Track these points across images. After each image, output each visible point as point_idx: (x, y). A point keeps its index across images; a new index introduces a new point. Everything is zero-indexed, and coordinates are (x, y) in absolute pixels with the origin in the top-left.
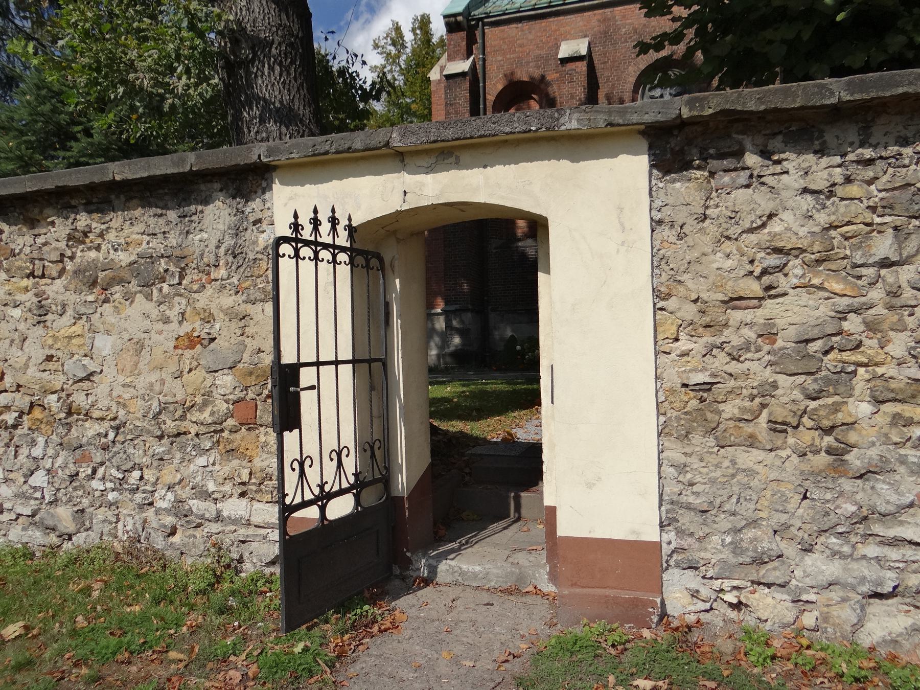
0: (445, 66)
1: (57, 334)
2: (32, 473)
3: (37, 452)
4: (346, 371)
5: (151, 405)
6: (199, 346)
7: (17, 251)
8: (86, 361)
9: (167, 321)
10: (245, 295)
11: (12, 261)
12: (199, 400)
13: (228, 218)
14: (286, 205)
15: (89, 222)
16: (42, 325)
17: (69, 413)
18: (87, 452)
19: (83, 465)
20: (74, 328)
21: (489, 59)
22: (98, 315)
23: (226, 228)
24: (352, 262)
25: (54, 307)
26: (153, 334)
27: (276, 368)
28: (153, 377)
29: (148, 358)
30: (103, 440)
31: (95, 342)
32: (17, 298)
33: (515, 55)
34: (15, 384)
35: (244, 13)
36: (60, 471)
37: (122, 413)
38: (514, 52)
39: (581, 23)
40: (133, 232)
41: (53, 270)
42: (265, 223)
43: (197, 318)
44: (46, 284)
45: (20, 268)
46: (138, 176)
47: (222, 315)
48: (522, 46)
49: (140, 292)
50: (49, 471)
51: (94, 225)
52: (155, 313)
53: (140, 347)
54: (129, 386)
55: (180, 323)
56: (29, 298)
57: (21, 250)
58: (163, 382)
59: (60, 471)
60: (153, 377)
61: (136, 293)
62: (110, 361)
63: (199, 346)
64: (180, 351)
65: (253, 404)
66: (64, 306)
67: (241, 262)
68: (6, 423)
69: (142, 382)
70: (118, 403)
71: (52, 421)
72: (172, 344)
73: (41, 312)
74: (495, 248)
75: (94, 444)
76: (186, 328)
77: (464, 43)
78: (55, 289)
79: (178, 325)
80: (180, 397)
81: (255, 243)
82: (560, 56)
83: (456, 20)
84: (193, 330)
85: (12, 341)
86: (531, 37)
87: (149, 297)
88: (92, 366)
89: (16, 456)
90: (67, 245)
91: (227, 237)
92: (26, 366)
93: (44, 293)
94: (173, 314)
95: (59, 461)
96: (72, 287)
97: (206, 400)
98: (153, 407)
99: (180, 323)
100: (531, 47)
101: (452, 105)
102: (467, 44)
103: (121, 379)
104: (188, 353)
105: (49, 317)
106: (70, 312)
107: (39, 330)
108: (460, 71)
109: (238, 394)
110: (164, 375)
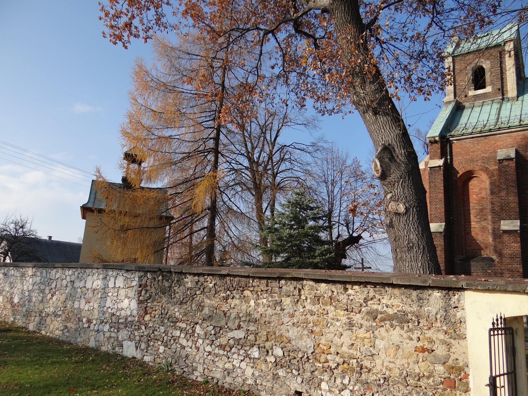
0: (428, 162)
1: (358, 336)
2: (343, 390)
3: (346, 381)
4: (506, 376)
5: (403, 372)
6: (427, 352)
7: (340, 300)
8: (371, 349)
9: (411, 339)
10: (450, 335)
11: (337, 303)
12: (426, 374)
13: (441, 304)
14: (471, 304)
15: (374, 294)
16: (350, 331)
17: (361, 369)
18: (370, 386)
19: (368, 391)
20: (365, 335)
21: (454, 158)
22: (378, 331)
23: (440, 307)
24: (505, 334)
25: (356, 325)
26: (404, 343)
27: (492, 378)
28: (404, 361)
29: (402, 353)
30: (378, 382)
31: (376, 342)
32: (338, 318)
33: (470, 157)
34: (336, 352)
35: (401, 194)
36: (357, 392)
37: (387, 373)
38: (469, 155)
39: (510, 140)
40: (396, 302)
41: (356, 310)
42: (459, 309)
43: (426, 340)
44: (353, 315)
45: (341, 306)
46: (404, 284)
47: (438, 342)
48: (474, 151)
49: (398, 326)
50: (351, 391)
51: (377, 296)
52: (405, 335)
53: (398, 347)
54: (392, 362)
55: (418, 341)
56: (344, 319)
57: (342, 300)
58: (409, 364)
59: (357, 392)
60: (404, 361)
61: (396, 326)
62: (383, 350)
63: (427, 352)
64: (417, 353)
65: (453, 381)
66: (362, 325)
67: (448, 322)
68: (331, 367)
69: (399, 362)
70: (387, 369)
71: (353, 370)
72: (413, 350)
73: (351, 325)
74: (460, 260)
75: (374, 384)
76: (420, 344)
77: (439, 151)
78: (357, 318)
79: (416, 342)
80: (417, 371)
81: (455, 315)
82: (498, 158)
83: (435, 139)
84: (424, 345)
85: (335, 335)
86: (478, 147)
87: (402, 328)
88: (374, 352)
89: (335, 381)
90: (364, 302)
91: (441, 311)
92: (342, 345)
93: (352, 318)
94: (415, 337)
95: (356, 388)
96: (366, 318)
97: (430, 375)
98: (404, 373)
99: (418, 341)
100: (479, 153)
101: (433, 182)
102: (441, 151)
103: (388, 359)
104: (421, 355)
105: (354, 328)
106: (364, 328)
107: (349, 332)
108: (437, 165)
109: (447, 375)
110: (409, 361)
